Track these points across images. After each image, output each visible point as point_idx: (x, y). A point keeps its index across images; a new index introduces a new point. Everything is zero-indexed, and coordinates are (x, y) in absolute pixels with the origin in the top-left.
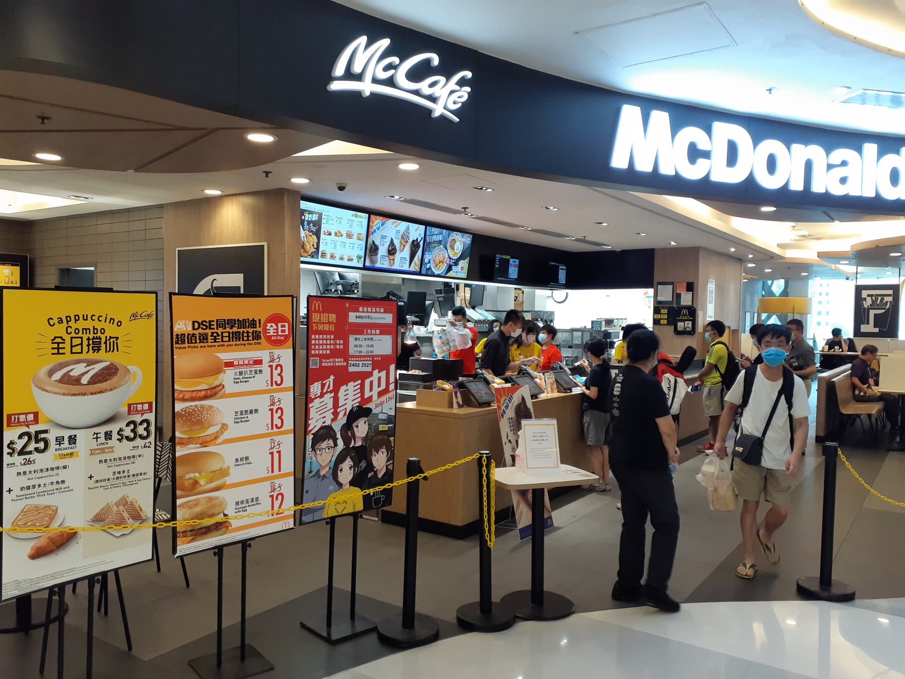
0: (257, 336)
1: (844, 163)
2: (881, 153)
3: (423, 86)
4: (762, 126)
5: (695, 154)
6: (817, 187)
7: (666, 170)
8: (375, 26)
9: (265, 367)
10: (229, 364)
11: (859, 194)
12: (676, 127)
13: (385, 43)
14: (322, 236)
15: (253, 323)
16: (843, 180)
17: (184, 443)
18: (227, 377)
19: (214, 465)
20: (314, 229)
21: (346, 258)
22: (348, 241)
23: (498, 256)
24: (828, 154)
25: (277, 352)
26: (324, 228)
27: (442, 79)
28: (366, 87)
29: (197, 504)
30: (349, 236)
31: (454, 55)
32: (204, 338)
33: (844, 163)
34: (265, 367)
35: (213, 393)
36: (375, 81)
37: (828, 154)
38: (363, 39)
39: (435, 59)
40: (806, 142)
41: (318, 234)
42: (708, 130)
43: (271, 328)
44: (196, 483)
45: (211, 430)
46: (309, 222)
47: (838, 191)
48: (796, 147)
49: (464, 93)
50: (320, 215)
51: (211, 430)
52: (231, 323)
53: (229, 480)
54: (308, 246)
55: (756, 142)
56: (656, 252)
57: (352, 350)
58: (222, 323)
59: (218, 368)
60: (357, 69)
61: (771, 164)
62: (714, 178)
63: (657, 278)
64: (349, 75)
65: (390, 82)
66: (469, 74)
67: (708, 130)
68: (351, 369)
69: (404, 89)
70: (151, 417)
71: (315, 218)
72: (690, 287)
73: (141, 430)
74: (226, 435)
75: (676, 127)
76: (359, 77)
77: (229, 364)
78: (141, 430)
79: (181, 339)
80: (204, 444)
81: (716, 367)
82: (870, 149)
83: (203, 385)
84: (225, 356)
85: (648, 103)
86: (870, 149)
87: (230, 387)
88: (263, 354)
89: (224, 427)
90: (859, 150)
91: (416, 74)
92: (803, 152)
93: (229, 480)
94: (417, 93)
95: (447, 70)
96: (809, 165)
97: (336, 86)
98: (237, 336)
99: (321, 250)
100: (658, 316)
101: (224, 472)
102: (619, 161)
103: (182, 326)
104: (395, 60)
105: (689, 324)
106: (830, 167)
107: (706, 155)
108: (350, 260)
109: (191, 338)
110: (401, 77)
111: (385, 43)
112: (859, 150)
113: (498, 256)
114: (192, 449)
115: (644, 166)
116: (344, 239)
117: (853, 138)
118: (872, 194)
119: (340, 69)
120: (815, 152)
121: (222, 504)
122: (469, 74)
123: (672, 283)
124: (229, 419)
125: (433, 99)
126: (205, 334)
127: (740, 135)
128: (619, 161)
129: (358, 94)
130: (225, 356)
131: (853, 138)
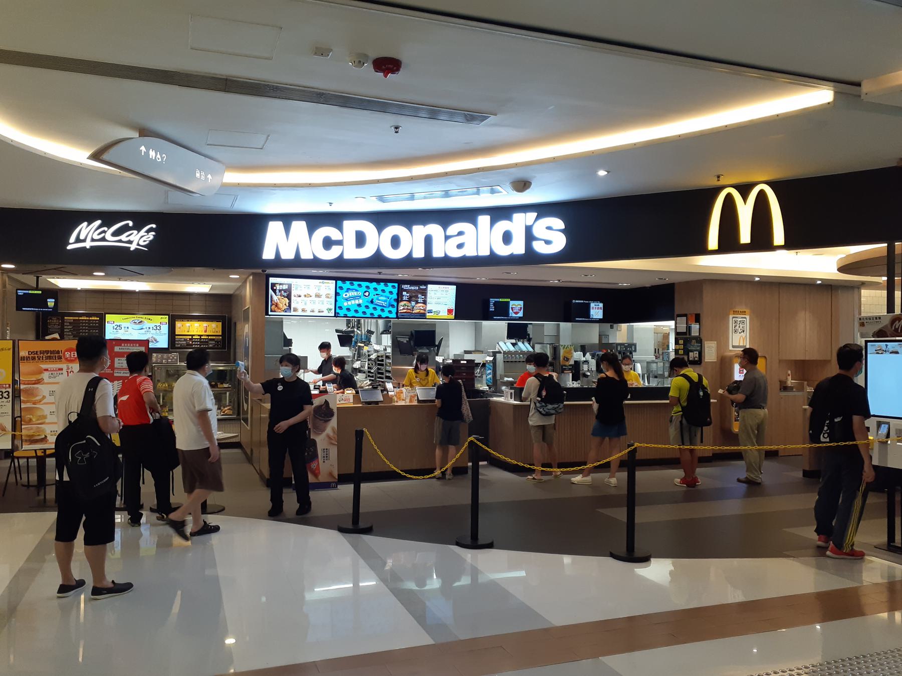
0: (60, 358)
1: (460, 233)
2: (493, 222)
3: (123, 237)
4: (381, 219)
5: (328, 243)
6: (437, 253)
7: (306, 255)
8: (89, 216)
9: (64, 372)
10: (47, 370)
11: (475, 254)
12: (311, 230)
13: (99, 222)
14: (293, 298)
15: (58, 352)
16: (460, 246)
17: (25, 402)
18: (45, 376)
19: (39, 413)
20: (285, 294)
21: (316, 311)
22: (317, 299)
23: (492, 300)
24: (445, 229)
25: (70, 365)
26: (294, 292)
27: (135, 232)
28: (88, 244)
29: (32, 429)
30: (318, 296)
31: (140, 219)
32: (34, 358)
33: (460, 233)
34: (64, 372)
35: (38, 382)
36: (93, 240)
37: (445, 229)
38: (85, 224)
39: (131, 223)
40: (424, 223)
41: (289, 297)
42: (340, 228)
43: (67, 354)
44: (31, 419)
45: (38, 398)
46: (280, 291)
47: (455, 253)
48: (417, 229)
49: (151, 236)
50: (290, 286)
51: (38, 398)
52: (47, 352)
53: (47, 421)
54: (281, 305)
55: (380, 229)
56: (676, 288)
57: (116, 365)
58: (42, 352)
59: (41, 371)
60: (82, 237)
61: (395, 242)
62: (346, 257)
63: (677, 312)
64: (78, 240)
65: (103, 239)
66: (154, 226)
67: (340, 228)
68: (116, 375)
69: (111, 240)
70: (10, 390)
71: (285, 287)
72: (698, 319)
73: (5, 395)
74: (45, 401)
75: (311, 230)
76: (84, 241)
77: (47, 370)
78: (5, 395)
79: (23, 358)
80: (34, 403)
81: (679, 400)
82: (484, 220)
83: (34, 378)
84: (44, 366)
85: (287, 219)
86: (484, 220)
87: (46, 380)
88: (64, 366)
89: (44, 397)
90: (474, 222)
91: (116, 233)
92: (420, 231)
93: (47, 421)
94: (120, 241)
95: (138, 227)
96: (428, 240)
97: (69, 247)
98: (50, 358)
99: (292, 306)
100: (678, 347)
101: (45, 417)
102: (268, 254)
103: (23, 353)
104: (106, 229)
105: (696, 354)
106: (447, 238)
107: (340, 243)
108: (313, 311)
109: (27, 358)
110: (108, 236)
111: (99, 222)
112: (474, 222)
113: (492, 300)
114: (29, 405)
115: (288, 254)
116: (313, 298)
117: (469, 215)
118: (487, 253)
119: (72, 239)
120: (434, 229)
121: (43, 431)
122: (154, 226)
123: (685, 315)
124: (46, 394)
125: (130, 242)
126: (34, 357)
127: (367, 227)
128: (268, 254)
129: (85, 248)
130: (44, 366)
131: (469, 215)
